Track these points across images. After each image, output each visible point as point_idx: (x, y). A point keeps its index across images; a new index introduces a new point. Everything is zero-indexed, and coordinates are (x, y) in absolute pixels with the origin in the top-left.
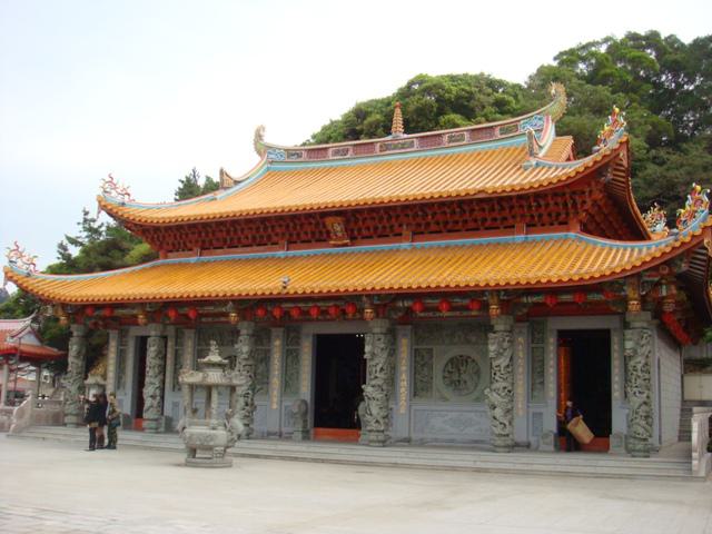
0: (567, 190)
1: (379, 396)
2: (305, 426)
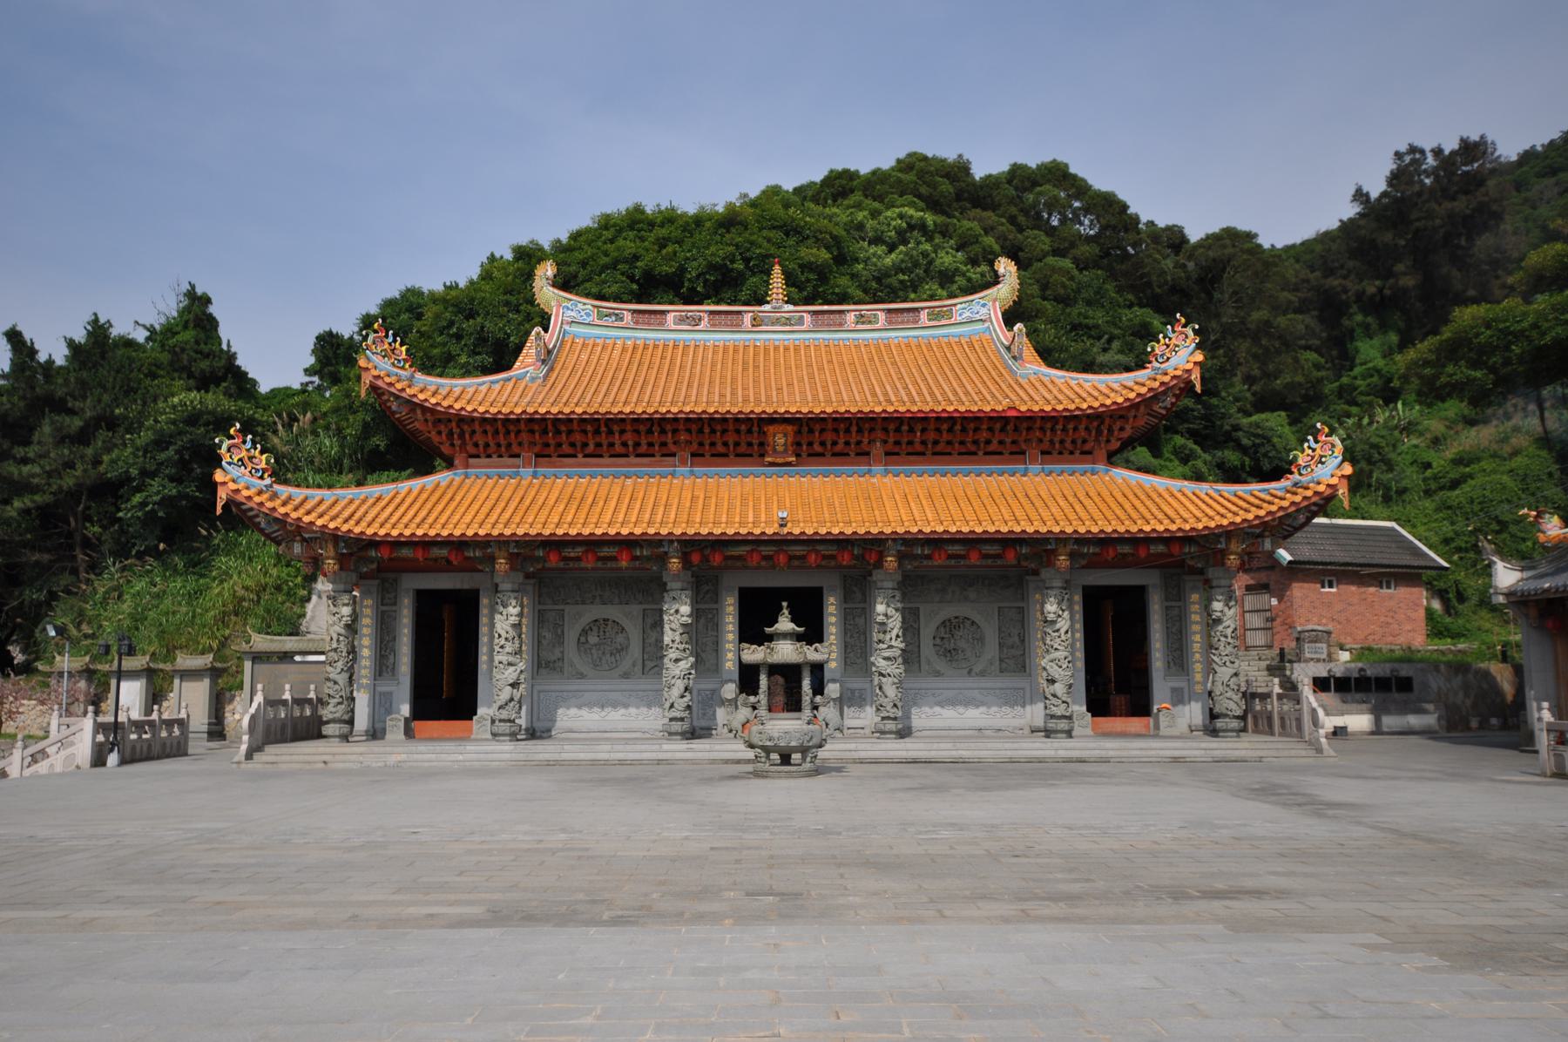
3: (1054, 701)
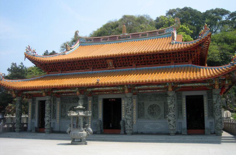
0: (189, 51)
1: (130, 118)
2: (101, 129)
3: (170, 126)
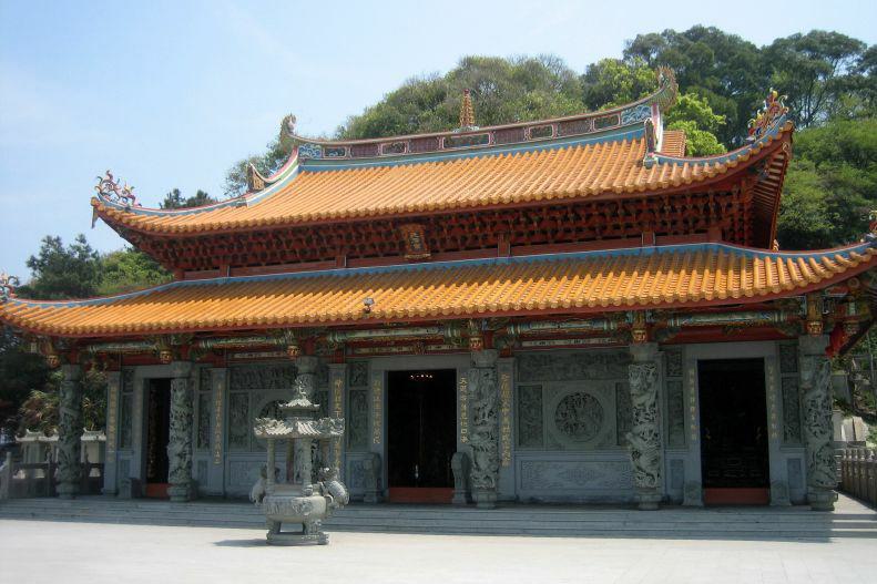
0: (710, 191)
1: (490, 445)
